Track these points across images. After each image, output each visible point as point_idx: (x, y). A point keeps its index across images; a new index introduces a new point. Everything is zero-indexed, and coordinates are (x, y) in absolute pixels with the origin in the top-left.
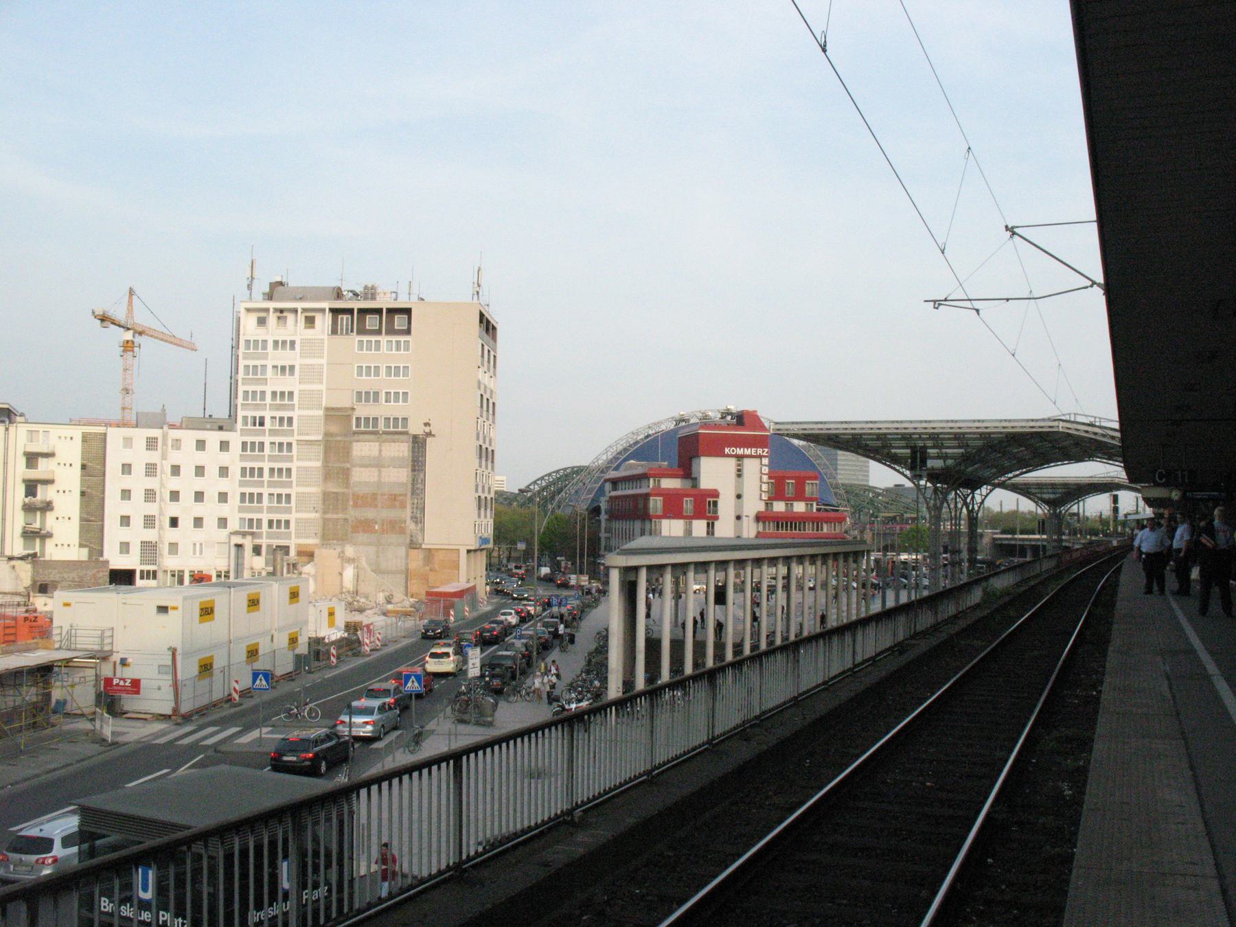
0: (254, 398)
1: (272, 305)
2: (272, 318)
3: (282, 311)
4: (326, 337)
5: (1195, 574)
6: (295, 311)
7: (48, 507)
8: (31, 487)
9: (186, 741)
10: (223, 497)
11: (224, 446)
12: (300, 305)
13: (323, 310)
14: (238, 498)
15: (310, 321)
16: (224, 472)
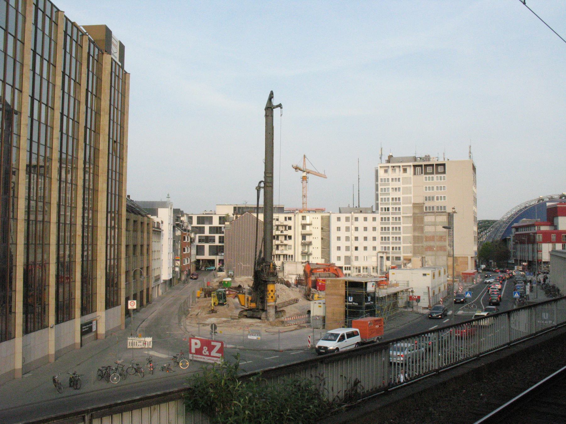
0: (385, 201)
1: (390, 165)
2: (390, 170)
3: (394, 167)
6: (399, 167)
7: (310, 244)
8: (304, 237)
10: (374, 239)
11: (374, 219)
14: (380, 239)
16: (374, 229)
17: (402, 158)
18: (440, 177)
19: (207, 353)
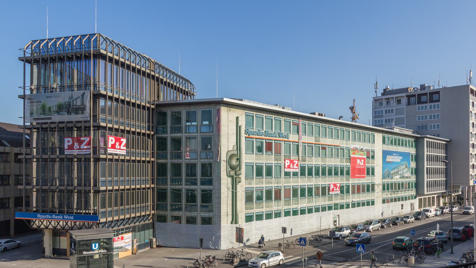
3: (388, 99)
4: (405, 107)
6: (393, 98)
9: (291, 256)
12: (394, 96)
13: (404, 96)
15: (399, 102)
17: (396, 90)
18: (434, 105)
19: (119, 147)
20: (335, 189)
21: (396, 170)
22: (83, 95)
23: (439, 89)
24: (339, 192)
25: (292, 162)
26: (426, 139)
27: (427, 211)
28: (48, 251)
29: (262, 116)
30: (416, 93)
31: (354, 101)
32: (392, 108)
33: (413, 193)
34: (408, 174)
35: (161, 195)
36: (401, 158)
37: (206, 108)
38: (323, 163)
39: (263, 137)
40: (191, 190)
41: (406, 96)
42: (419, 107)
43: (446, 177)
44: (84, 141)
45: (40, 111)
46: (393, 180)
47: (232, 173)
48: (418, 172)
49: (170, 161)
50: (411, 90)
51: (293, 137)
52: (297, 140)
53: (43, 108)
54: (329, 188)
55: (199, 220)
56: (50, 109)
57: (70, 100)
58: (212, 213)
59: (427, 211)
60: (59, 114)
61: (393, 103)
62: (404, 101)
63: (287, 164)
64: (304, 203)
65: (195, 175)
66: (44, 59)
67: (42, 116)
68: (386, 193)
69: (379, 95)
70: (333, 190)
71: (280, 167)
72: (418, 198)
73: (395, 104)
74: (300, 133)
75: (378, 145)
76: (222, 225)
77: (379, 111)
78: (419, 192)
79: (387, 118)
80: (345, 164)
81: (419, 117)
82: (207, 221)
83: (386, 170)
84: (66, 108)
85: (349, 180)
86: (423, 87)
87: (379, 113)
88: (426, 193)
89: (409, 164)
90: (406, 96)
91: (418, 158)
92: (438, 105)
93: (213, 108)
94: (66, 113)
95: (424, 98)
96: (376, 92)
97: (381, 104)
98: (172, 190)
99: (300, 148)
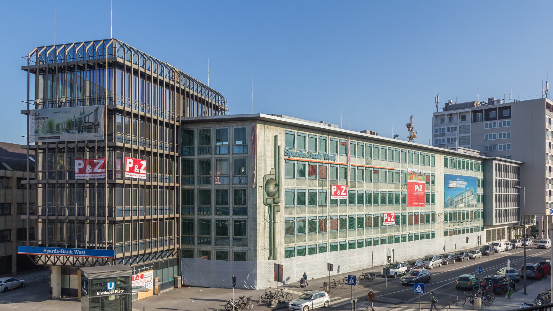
3: (451, 115)
4: (470, 124)
5: (243, 170)
6: (457, 114)
9: (338, 297)
12: (458, 111)
13: (469, 112)
15: (463, 118)
17: (460, 104)
18: (505, 122)
19: (138, 171)
20: (389, 220)
21: (460, 198)
22: (97, 110)
23: (510, 103)
24: (394, 223)
25: (339, 188)
26: (494, 162)
27: (497, 245)
28: (56, 291)
29: (304, 135)
30: (484, 108)
31: (411, 117)
32: (455, 126)
33: (480, 223)
34: (475, 202)
35: (188, 227)
36: (466, 183)
37: (240, 125)
38: (375, 190)
39: (306, 159)
40: (222, 221)
41: (472, 111)
42: (487, 124)
43: (518, 205)
44: (98, 163)
45: (47, 129)
46: (457, 209)
47: (270, 201)
48: (485, 199)
49: (198, 187)
50: (477, 105)
51: (340, 159)
52: (345, 163)
53: (50, 125)
54: (382, 218)
55: (231, 256)
56: (58, 126)
57: (82, 116)
58: (247, 248)
59: (497, 245)
60: (69, 132)
61: (457, 119)
62: (470, 117)
63: (333, 191)
64: (353, 236)
65: (227, 204)
66: (51, 69)
67: (49, 135)
68: (448, 224)
69: (440, 110)
70: (387, 220)
71: (326, 193)
72: (485, 230)
73: (459, 120)
74: (349, 155)
75: (439, 169)
76: (258, 261)
77: (440, 129)
78: (487, 223)
79: (450, 137)
80: (401, 190)
81: (487, 136)
82: (240, 257)
83: (449, 197)
84: (76, 125)
85: (405, 209)
86: (491, 101)
87: (440, 131)
88: (495, 224)
89: (476, 191)
90: (472, 111)
91: (486, 183)
92: (509, 122)
93: (247, 126)
94: (77, 131)
95: (492, 114)
96: (437, 107)
97: (443, 121)
98: (200, 220)
99: (349, 172)
